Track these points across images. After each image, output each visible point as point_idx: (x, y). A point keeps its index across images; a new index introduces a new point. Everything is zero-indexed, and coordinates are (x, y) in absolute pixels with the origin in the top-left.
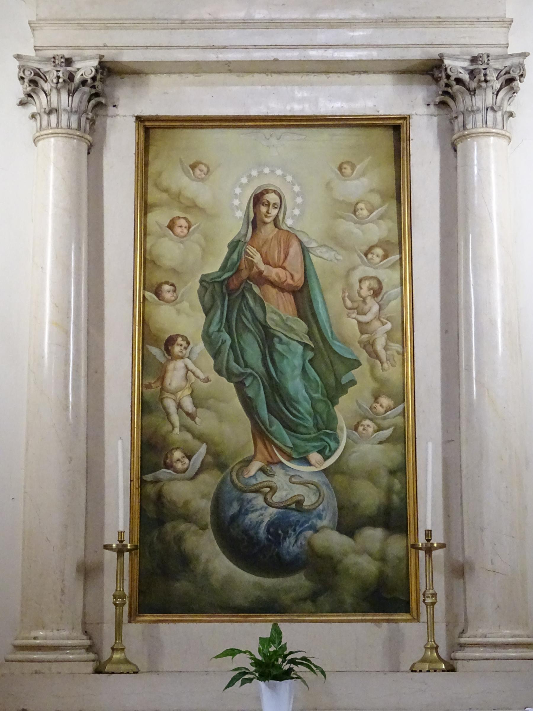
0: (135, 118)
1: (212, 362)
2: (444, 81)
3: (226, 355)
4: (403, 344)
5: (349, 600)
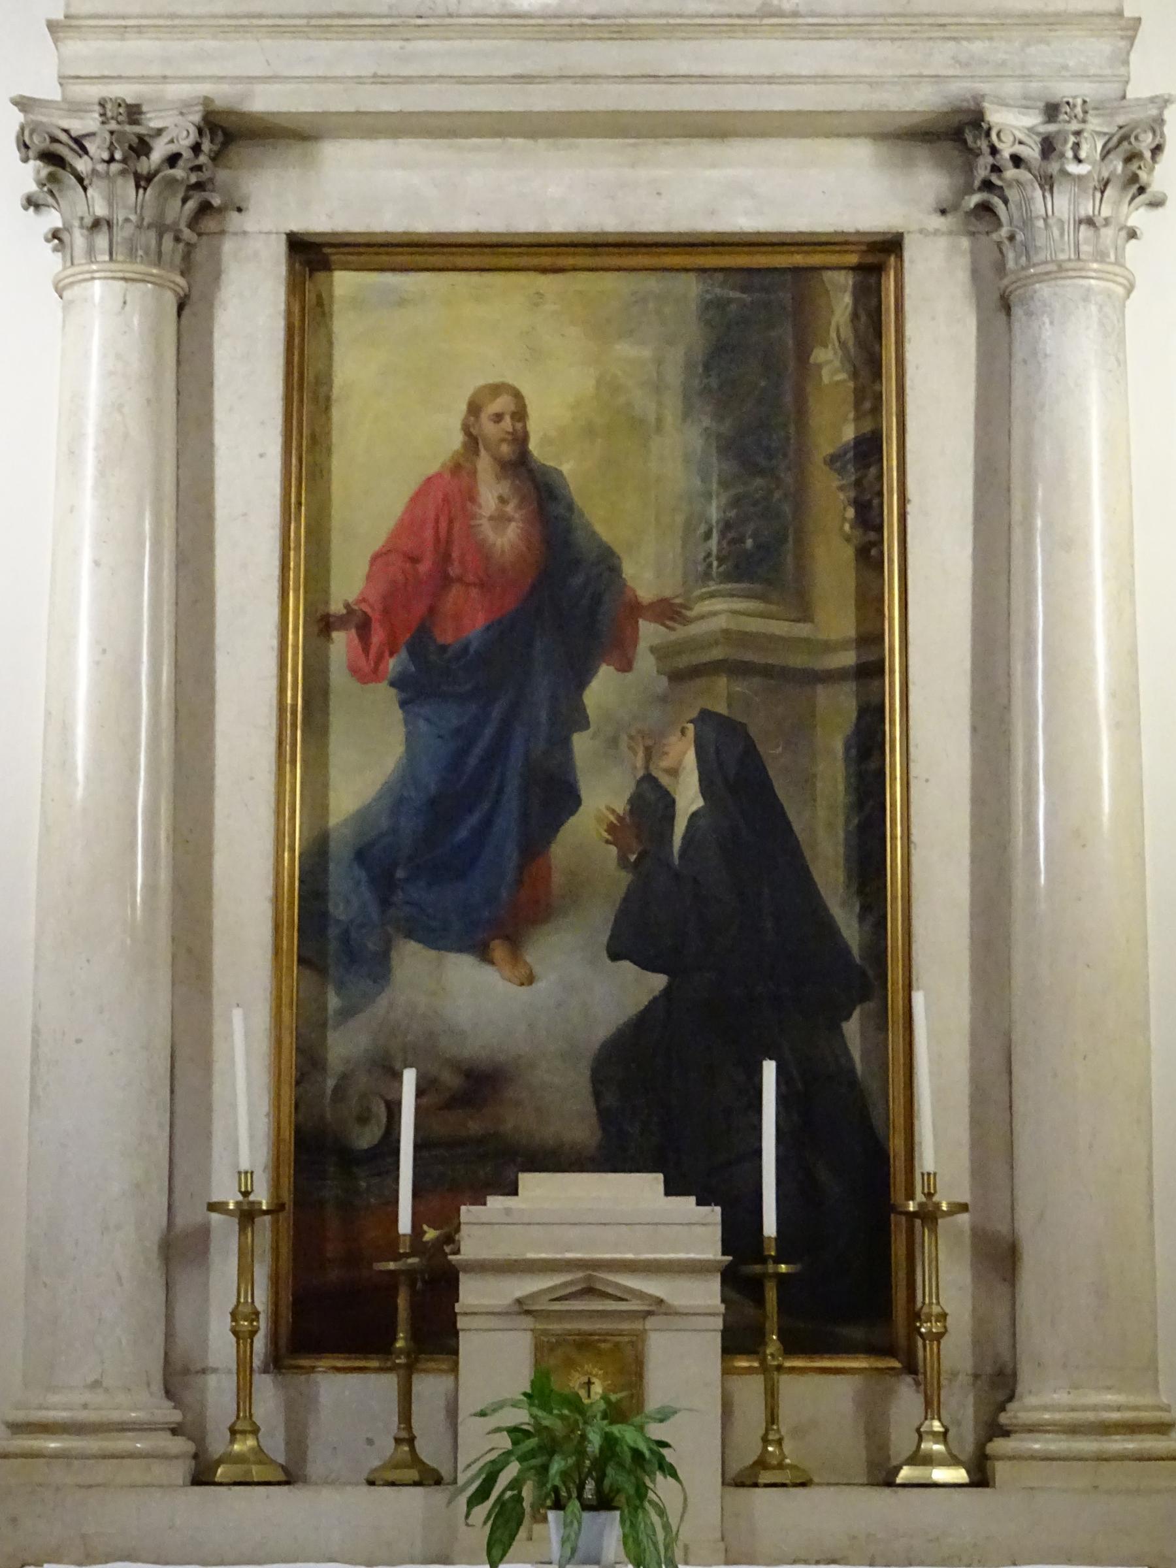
2: (986, 160)
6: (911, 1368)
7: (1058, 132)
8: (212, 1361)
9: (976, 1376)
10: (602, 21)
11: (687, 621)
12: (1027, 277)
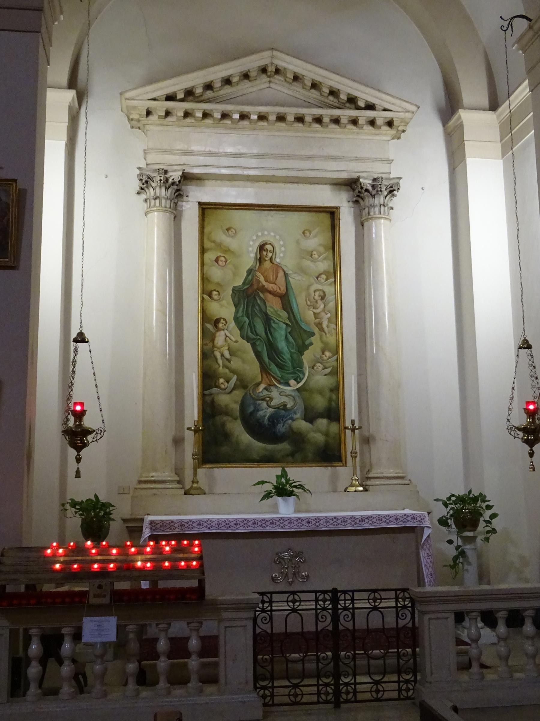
0: (198, 203)
1: (239, 332)
3: (246, 329)
4: (337, 325)
5: (310, 455)
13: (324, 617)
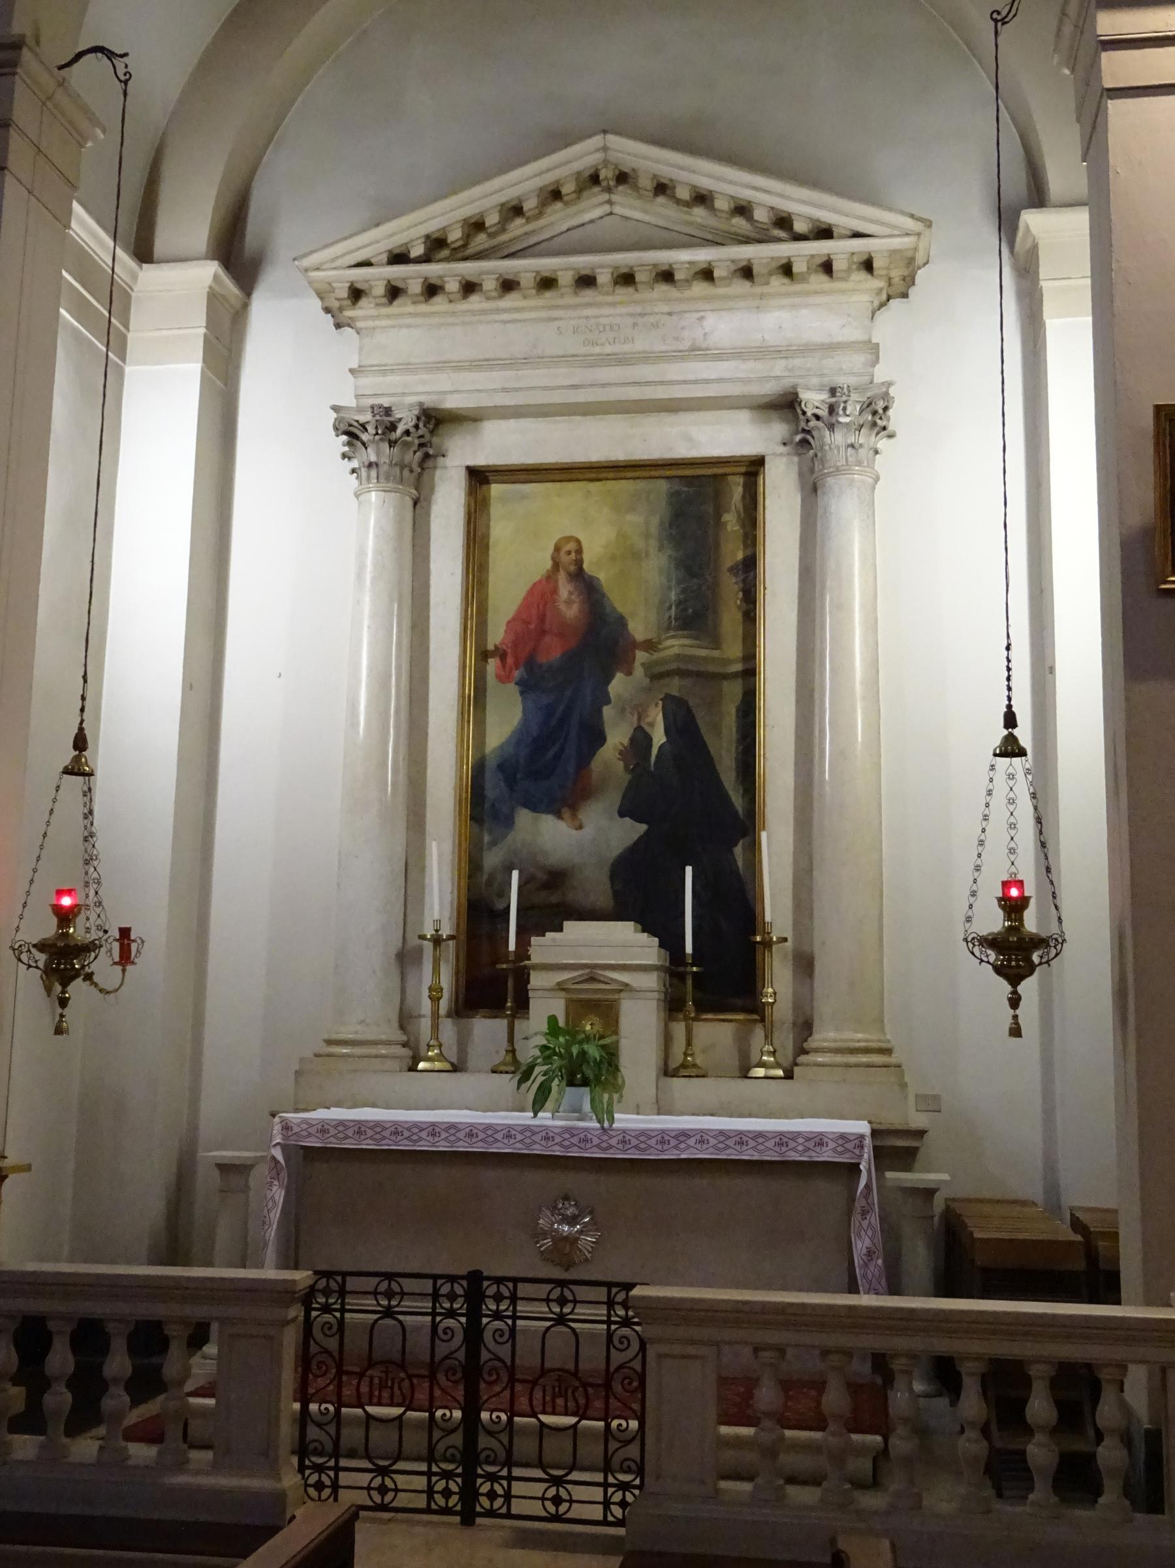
6: (763, 1020)
7: (836, 402)
8: (423, 1012)
9: (794, 1024)
10: (612, 357)
11: (659, 650)
12: (825, 474)
13: (450, 1333)
